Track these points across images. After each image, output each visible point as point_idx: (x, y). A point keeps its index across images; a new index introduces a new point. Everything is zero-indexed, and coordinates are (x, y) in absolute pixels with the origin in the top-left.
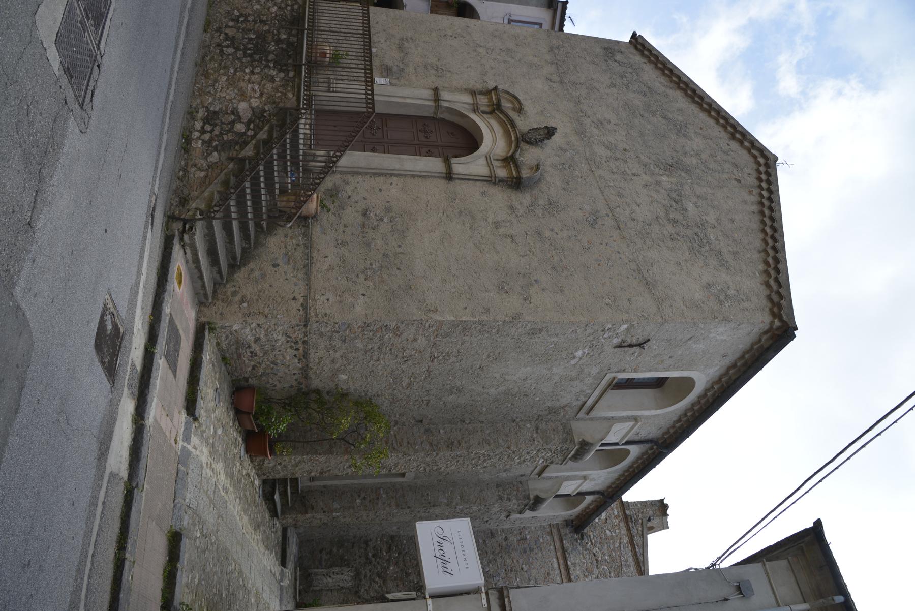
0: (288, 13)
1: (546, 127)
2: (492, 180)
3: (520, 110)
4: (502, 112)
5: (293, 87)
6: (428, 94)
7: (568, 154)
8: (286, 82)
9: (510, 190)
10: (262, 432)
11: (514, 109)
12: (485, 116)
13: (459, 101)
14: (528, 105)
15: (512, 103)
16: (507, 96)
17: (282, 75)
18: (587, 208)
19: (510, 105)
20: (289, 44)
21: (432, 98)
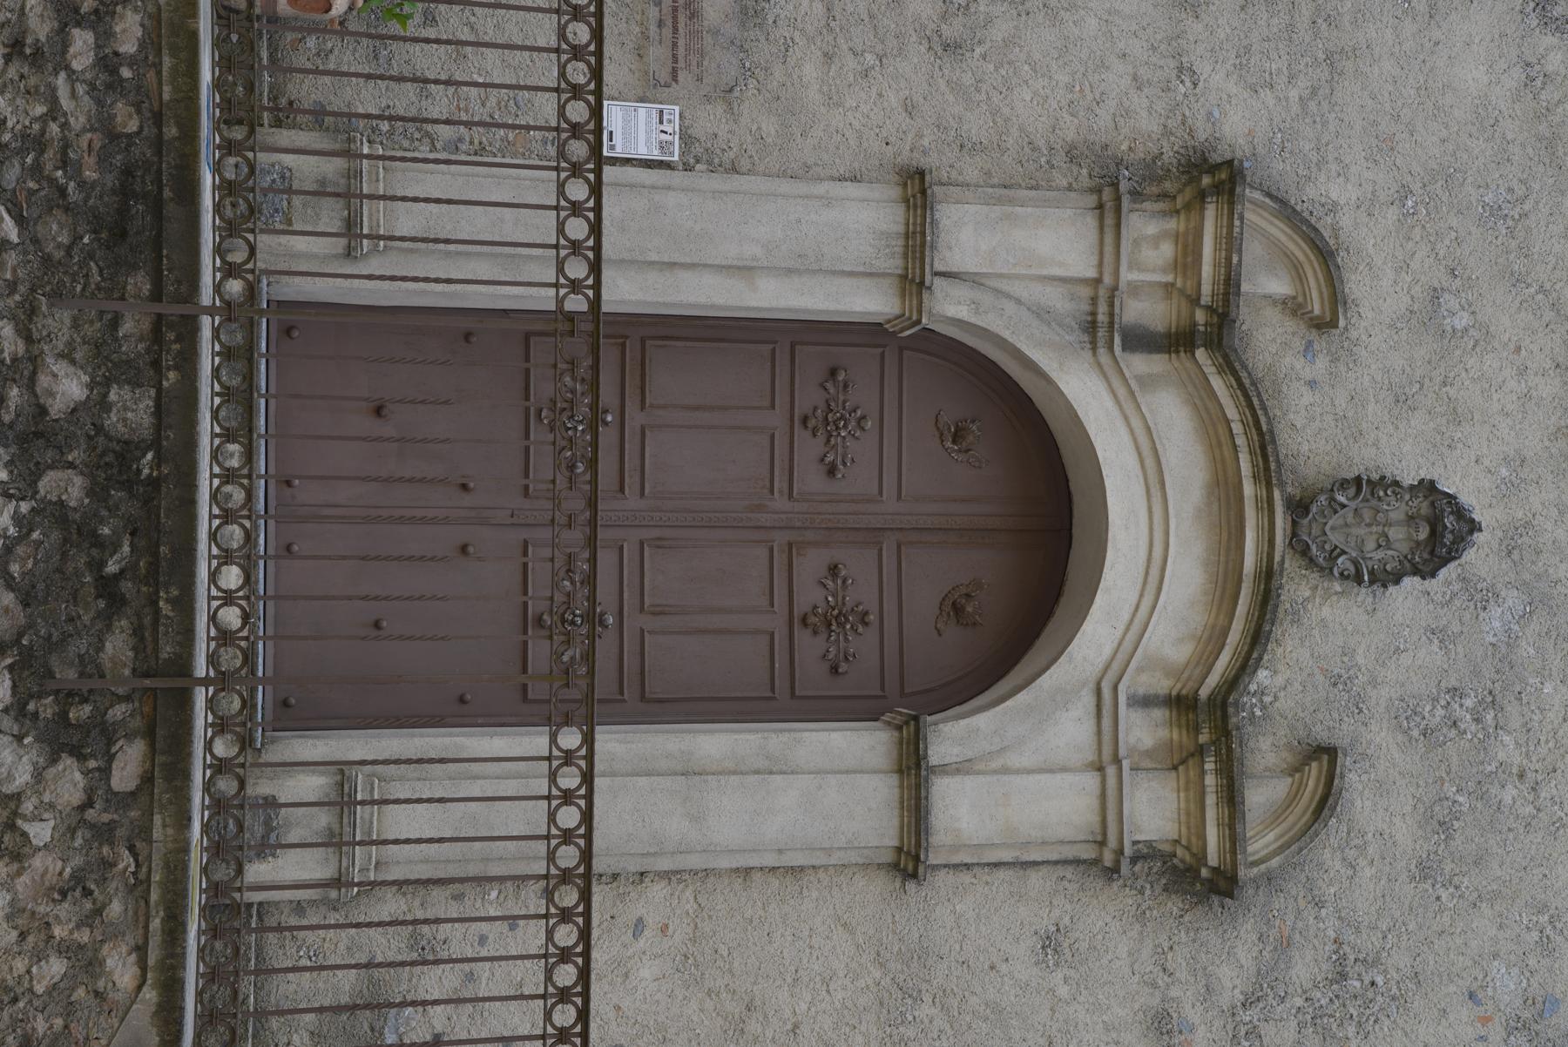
0: (77, 108)
1: (1428, 488)
2: (1104, 860)
3: (1324, 317)
4: (1230, 365)
5: (138, 888)
6: (869, 218)
7: (1495, 620)
8: (102, 826)
9: (1174, 905)
10: (38, 52)
11: (1294, 307)
12: (1139, 364)
13: (1017, 269)
14: (1378, 293)
15: (1298, 275)
16: (1279, 230)
17: (69, 782)
18: (1506, 985)
19: (1279, 286)
20: (113, 464)
21: (894, 264)
